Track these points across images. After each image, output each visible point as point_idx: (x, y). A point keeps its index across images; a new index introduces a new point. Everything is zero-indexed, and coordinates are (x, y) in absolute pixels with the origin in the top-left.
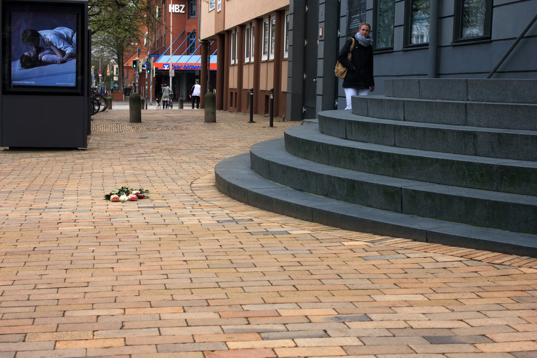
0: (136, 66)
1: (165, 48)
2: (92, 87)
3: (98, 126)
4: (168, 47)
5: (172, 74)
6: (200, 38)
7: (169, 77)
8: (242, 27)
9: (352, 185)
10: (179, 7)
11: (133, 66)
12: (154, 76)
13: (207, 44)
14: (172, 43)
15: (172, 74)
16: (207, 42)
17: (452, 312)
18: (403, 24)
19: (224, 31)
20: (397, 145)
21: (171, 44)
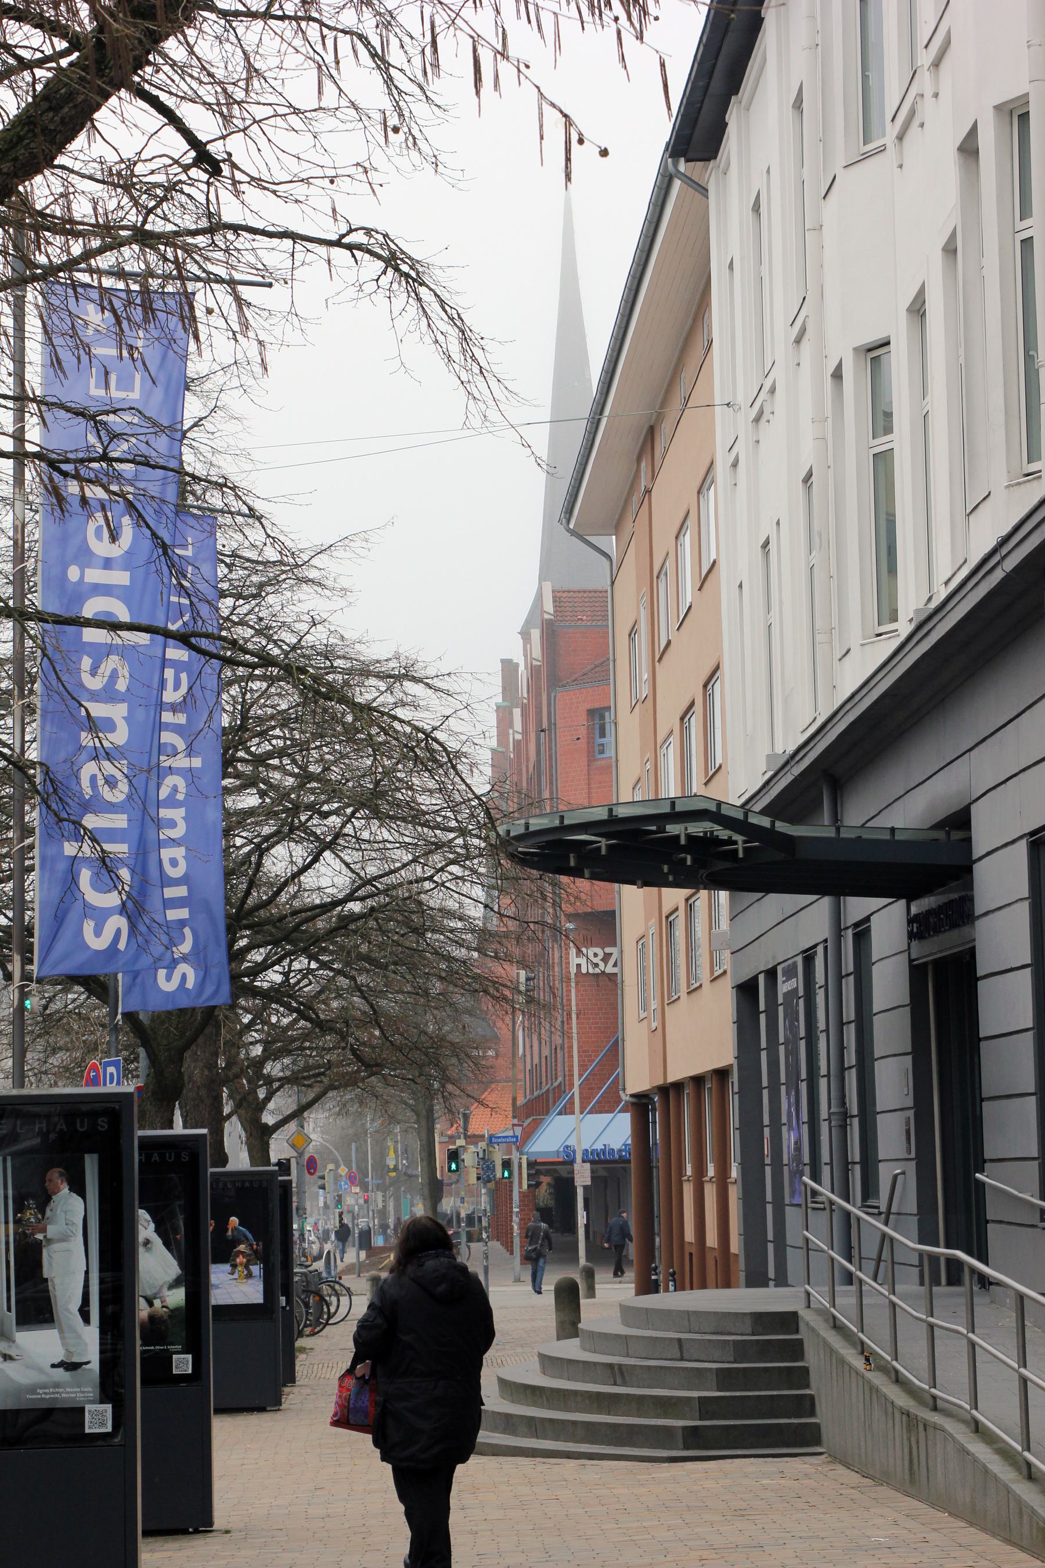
0: (457, 1166)
1: (559, 1091)
2: (265, 1071)
3: (316, 1367)
4: (570, 1090)
5: (583, 1176)
6: (624, 1090)
7: (574, 1188)
8: (698, 1081)
9: (530, 1421)
10: (601, 954)
11: (450, 1167)
12: (525, 1186)
13: (646, 1105)
14: (580, 1076)
15: (583, 1176)
16: (644, 1101)
17: (5, 1360)
18: (1031, 1025)
19: (665, 1083)
20: (352, 1422)
21: (577, 1083)
